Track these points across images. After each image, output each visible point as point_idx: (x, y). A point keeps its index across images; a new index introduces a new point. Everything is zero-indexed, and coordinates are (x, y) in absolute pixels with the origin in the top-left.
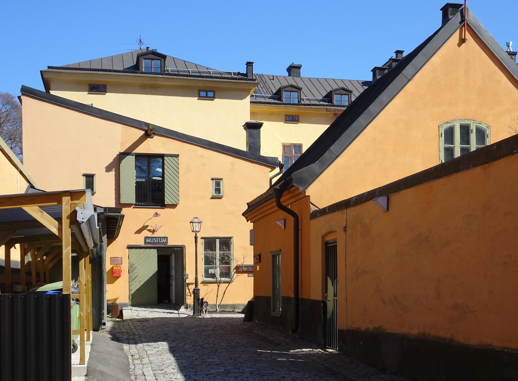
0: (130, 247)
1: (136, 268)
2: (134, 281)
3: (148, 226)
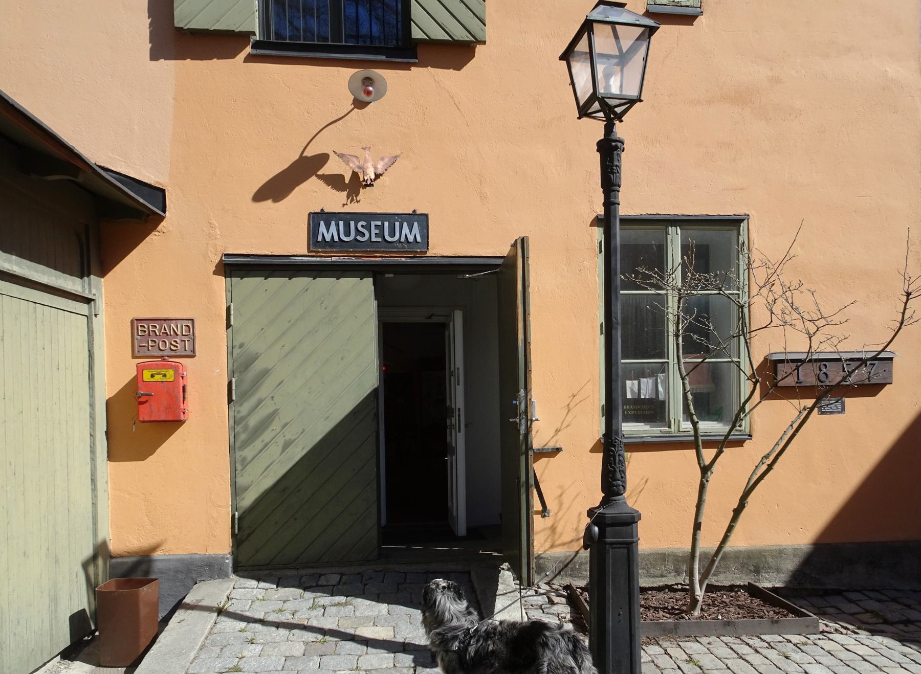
0: (234, 267)
1: (265, 373)
2: (258, 444)
3: (323, 159)
